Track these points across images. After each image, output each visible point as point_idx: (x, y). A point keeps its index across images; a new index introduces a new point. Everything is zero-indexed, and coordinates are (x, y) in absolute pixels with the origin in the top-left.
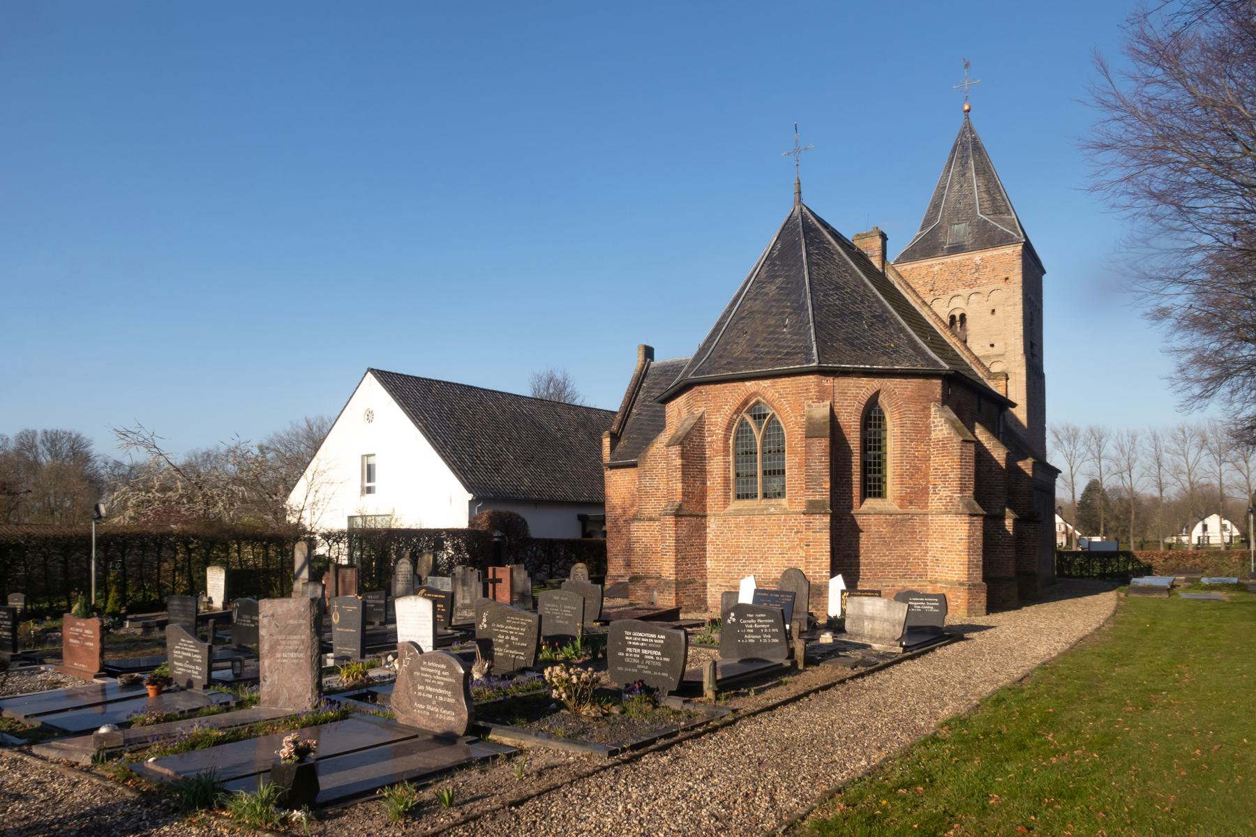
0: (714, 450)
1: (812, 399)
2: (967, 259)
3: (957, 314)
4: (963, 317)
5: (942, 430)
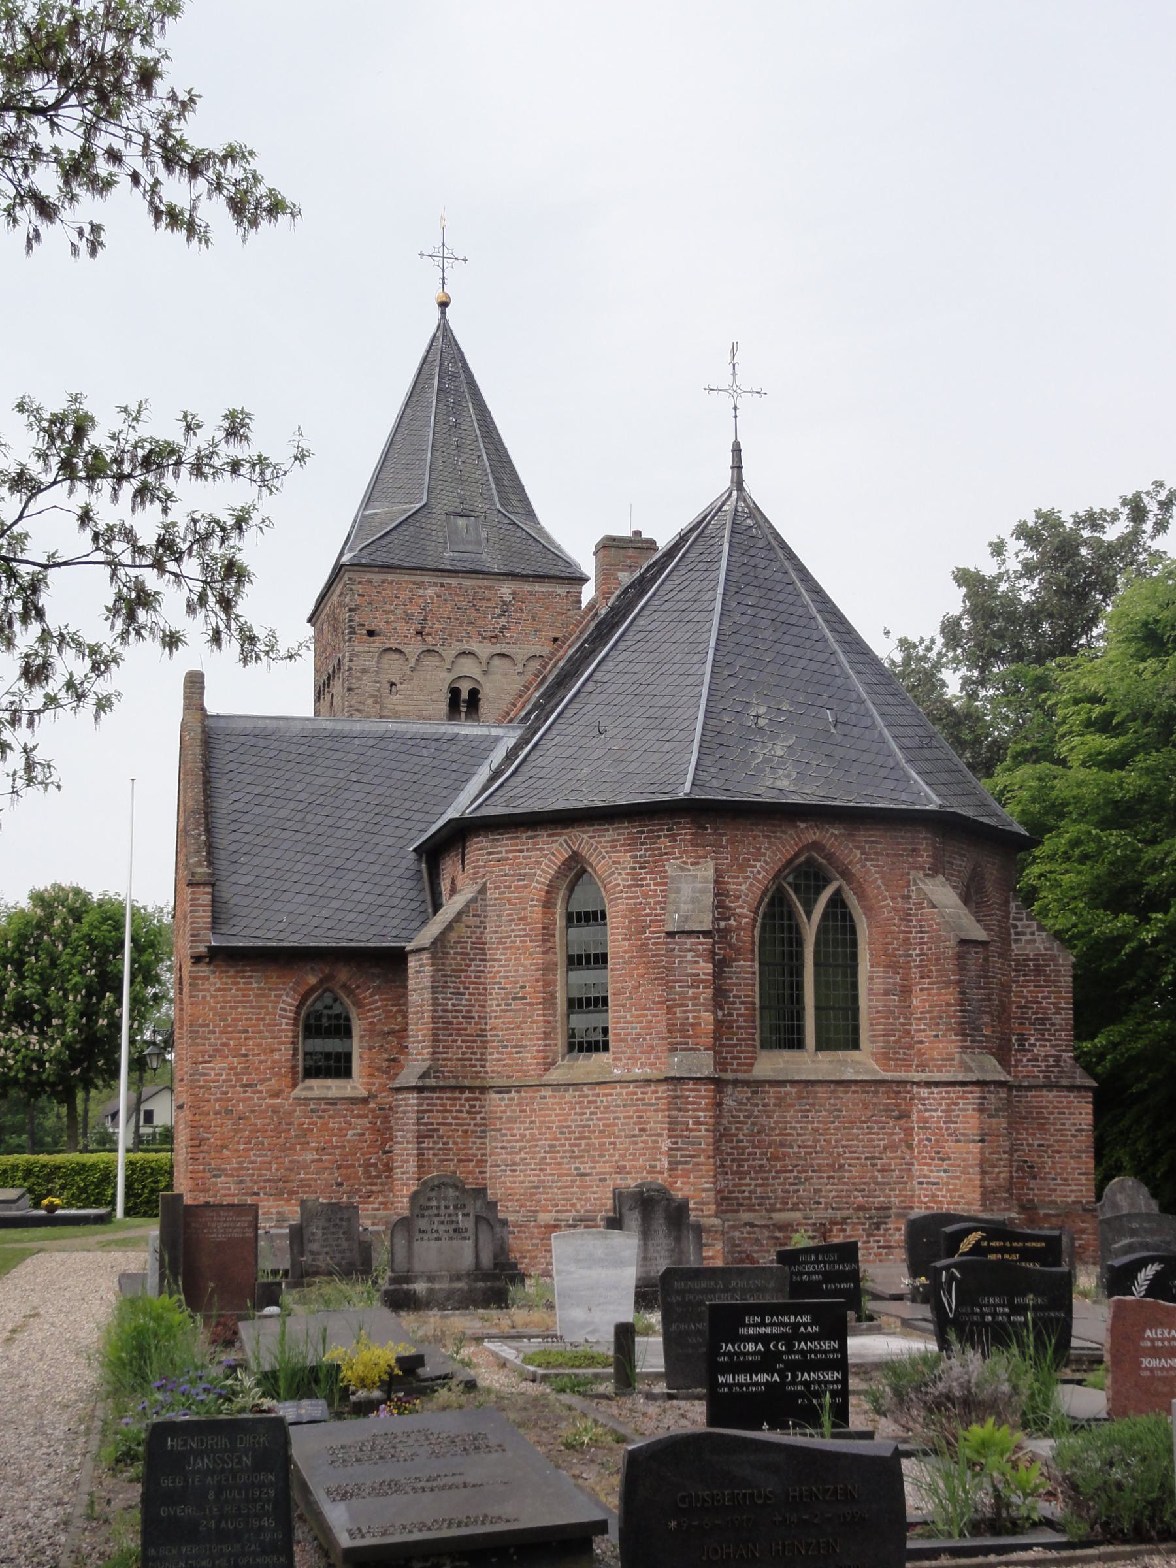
0: (731, 946)
1: (923, 868)
2: (486, 588)
3: (465, 688)
4: (474, 693)
5: (1034, 941)
